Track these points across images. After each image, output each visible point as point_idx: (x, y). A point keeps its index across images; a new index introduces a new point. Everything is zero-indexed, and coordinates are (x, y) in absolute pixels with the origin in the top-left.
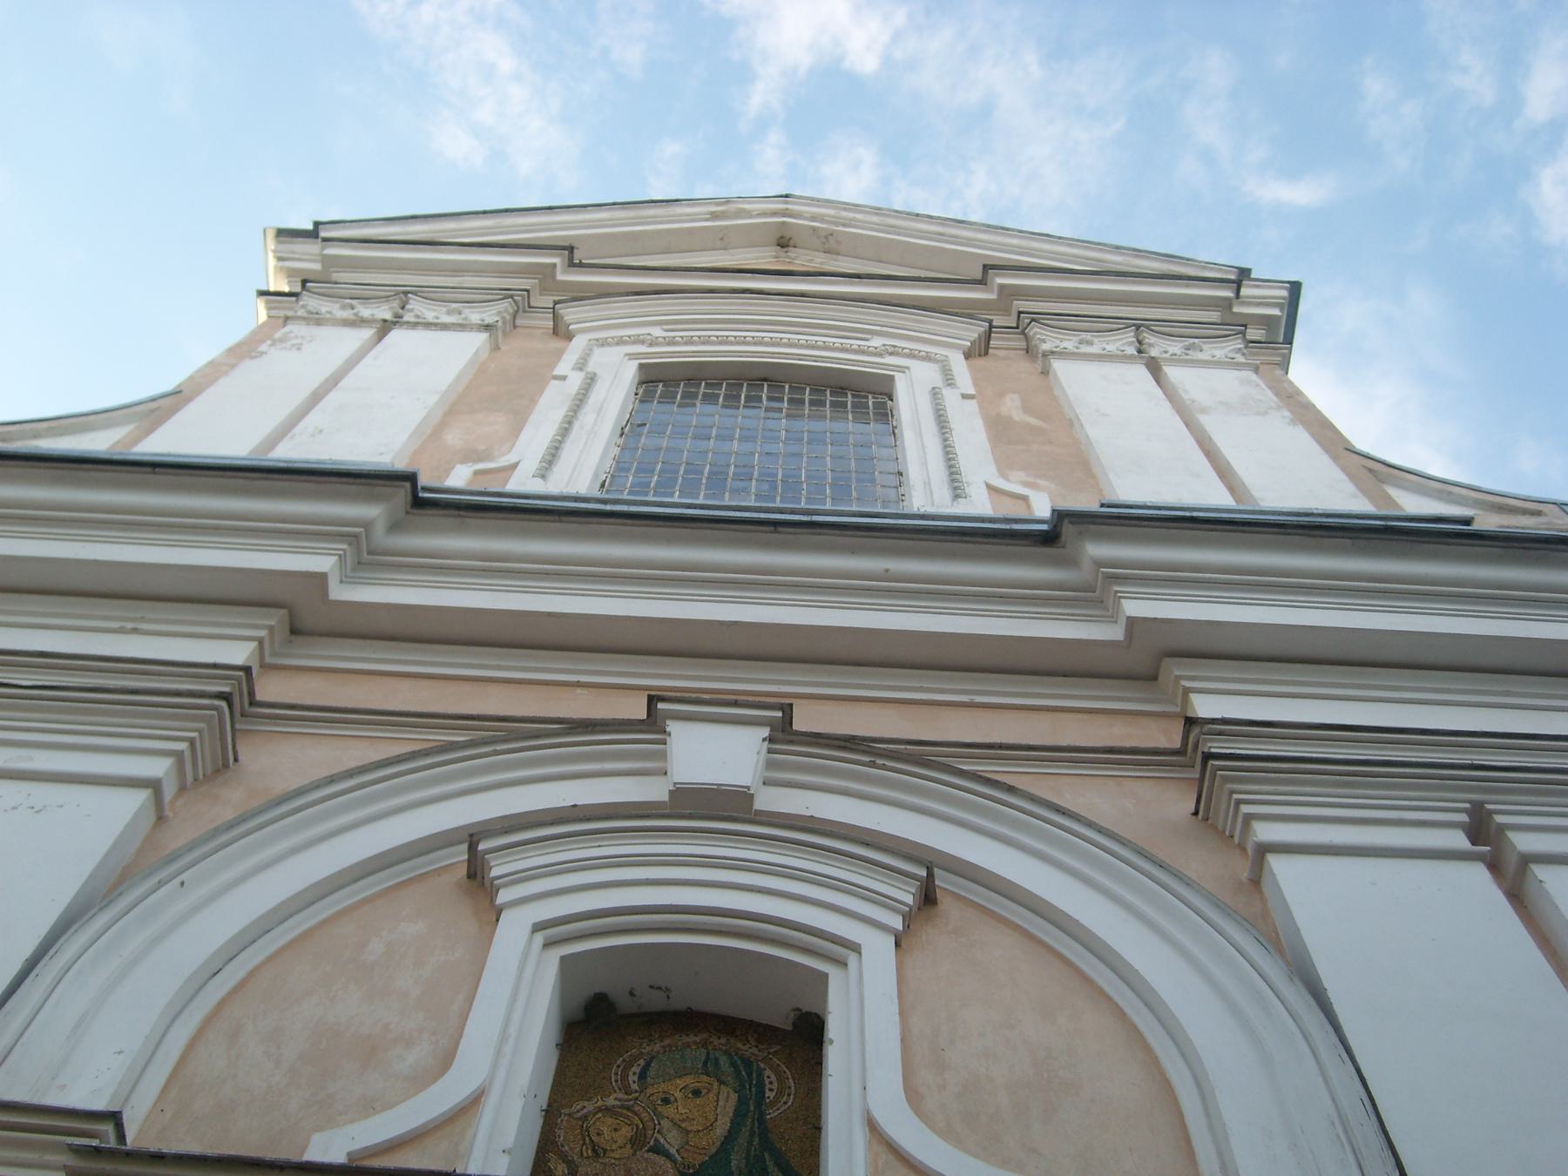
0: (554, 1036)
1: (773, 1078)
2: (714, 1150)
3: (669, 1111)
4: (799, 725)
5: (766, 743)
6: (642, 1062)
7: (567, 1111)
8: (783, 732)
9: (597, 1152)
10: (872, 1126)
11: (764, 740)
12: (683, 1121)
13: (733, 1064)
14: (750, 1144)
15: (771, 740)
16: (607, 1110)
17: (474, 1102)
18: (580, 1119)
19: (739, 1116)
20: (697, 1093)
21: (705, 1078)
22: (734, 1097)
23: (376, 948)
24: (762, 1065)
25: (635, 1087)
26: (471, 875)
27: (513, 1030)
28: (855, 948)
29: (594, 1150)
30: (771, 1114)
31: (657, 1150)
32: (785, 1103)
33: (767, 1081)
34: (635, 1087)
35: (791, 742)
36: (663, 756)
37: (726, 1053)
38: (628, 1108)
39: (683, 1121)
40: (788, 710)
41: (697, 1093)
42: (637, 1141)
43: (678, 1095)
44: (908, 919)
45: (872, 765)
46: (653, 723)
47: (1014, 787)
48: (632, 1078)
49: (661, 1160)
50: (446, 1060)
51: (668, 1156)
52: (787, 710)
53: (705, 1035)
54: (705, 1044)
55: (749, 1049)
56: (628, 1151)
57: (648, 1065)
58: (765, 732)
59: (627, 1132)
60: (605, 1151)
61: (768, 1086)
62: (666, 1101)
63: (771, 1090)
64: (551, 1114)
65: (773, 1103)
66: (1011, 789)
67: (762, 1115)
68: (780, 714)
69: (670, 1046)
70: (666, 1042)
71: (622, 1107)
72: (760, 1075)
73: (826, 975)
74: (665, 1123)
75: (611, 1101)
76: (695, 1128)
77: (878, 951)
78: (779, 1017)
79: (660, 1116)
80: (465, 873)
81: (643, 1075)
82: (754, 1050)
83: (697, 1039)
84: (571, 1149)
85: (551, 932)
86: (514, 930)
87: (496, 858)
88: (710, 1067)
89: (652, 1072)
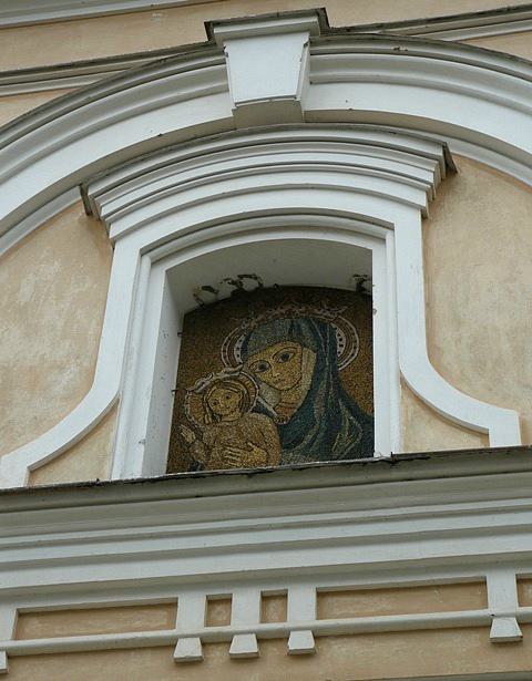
0: (173, 328)
1: (343, 335)
2: (300, 404)
3: (264, 376)
4: (334, 23)
5: (307, 48)
6: (243, 338)
7: (191, 389)
8: (324, 35)
9: (217, 418)
10: (404, 383)
11: (305, 45)
12: (276, 383)
13: (312, 329)
14: (327, 394)
15: (312, 43)
16: (220, 383)
17: (113, 409)
18: (200, 393)
19: (318, 371)
20: (285, 357)
21: (290, 344)
22: (314, 355)
23: (26, 291)
24: (334, 326)
25: (239, 360)
26: (89, 213)
27: (134, 345)
28: (390, 227)
29: (213, 417)
30: (343, 366)
31: (259, 410)
32: (353, 355)
33: (338, 338)
34: (239, 360)
35: (329, 42)
36: (224, 75)
37: (307, 319)
38: (235, 379)
39: (276, 383)
40: (322, 13)
41: (285, 357)
42: (244, 405)
43: (271, 361)
44: (431, 201)
45: (397, 52)
46: (211, 47)
47: (369, 312)
48: (237, 353)
49: (261, 417)
50: (89, 377)
51: (266, 413)
52: (321, 14)
53: (290, 307)
54: (289, 314)
55: (323, 314)
56: (237, 414)
57: (247, 339)
58: (305, 38)
59: (236, 399)
60: (221, 416)
61: (339, 343)
62: (263, 368)
63: (341, 346)
64: (180, 392)
65: (343, 357)
66: (513, 59)
67: (335, 367)
68: (315, 19)
69: (262, 320)
70: (260, 317)
71: (230, 379)
72: (332, 334)
73: (371, 251)
74: (263, 386)
75: (222, 375)
76: (285, 388)
77: (407, 225)
78: (346, 283)
79: (259, 381)
80: (84, 211)
81: (244, 349)
82: (328, 314)
83: (283, 311)
84: (196, 419)
85: (155, 253)
86: (126, 257)
87: (105, 198)
88: (294, 334)
89: (251, 345)
